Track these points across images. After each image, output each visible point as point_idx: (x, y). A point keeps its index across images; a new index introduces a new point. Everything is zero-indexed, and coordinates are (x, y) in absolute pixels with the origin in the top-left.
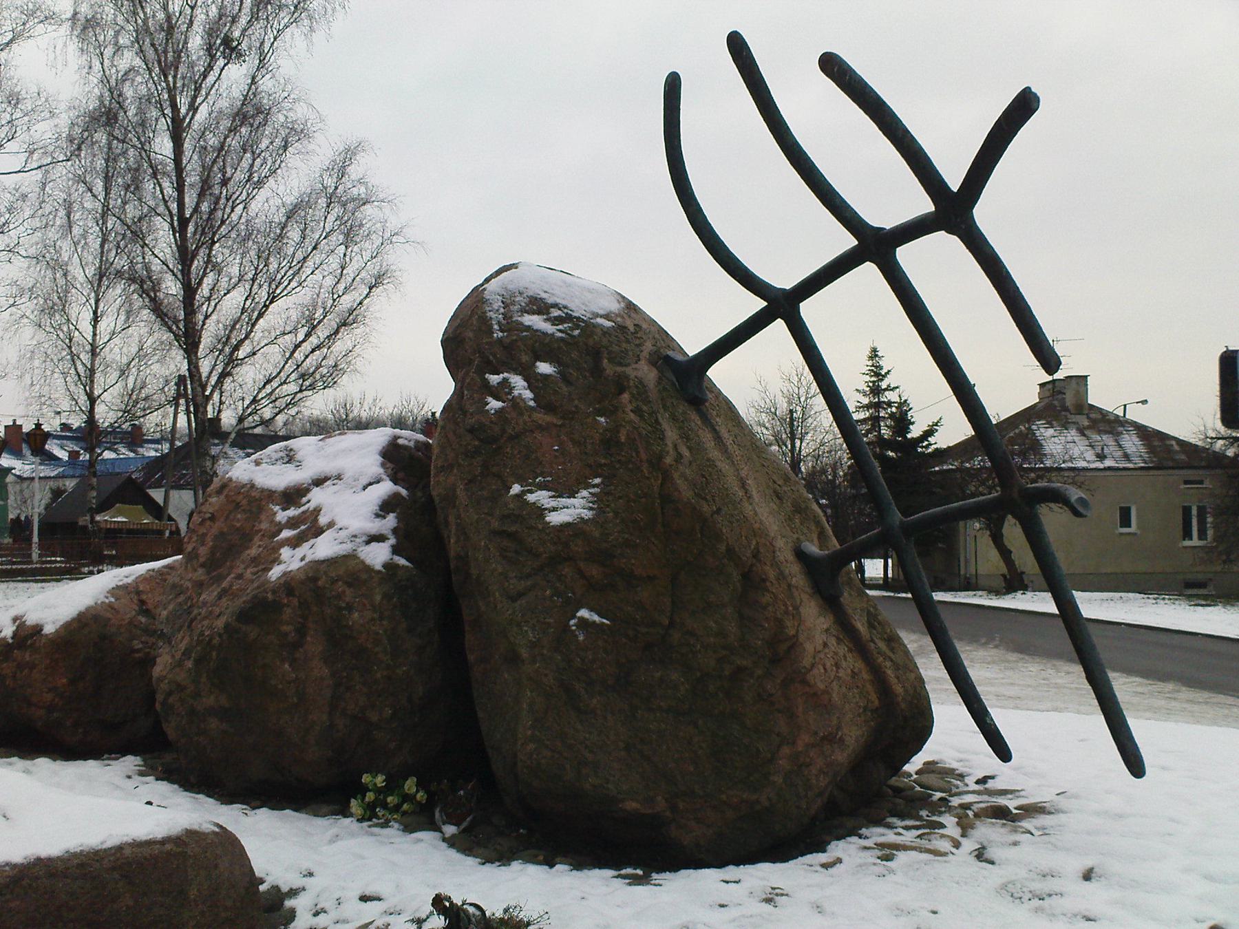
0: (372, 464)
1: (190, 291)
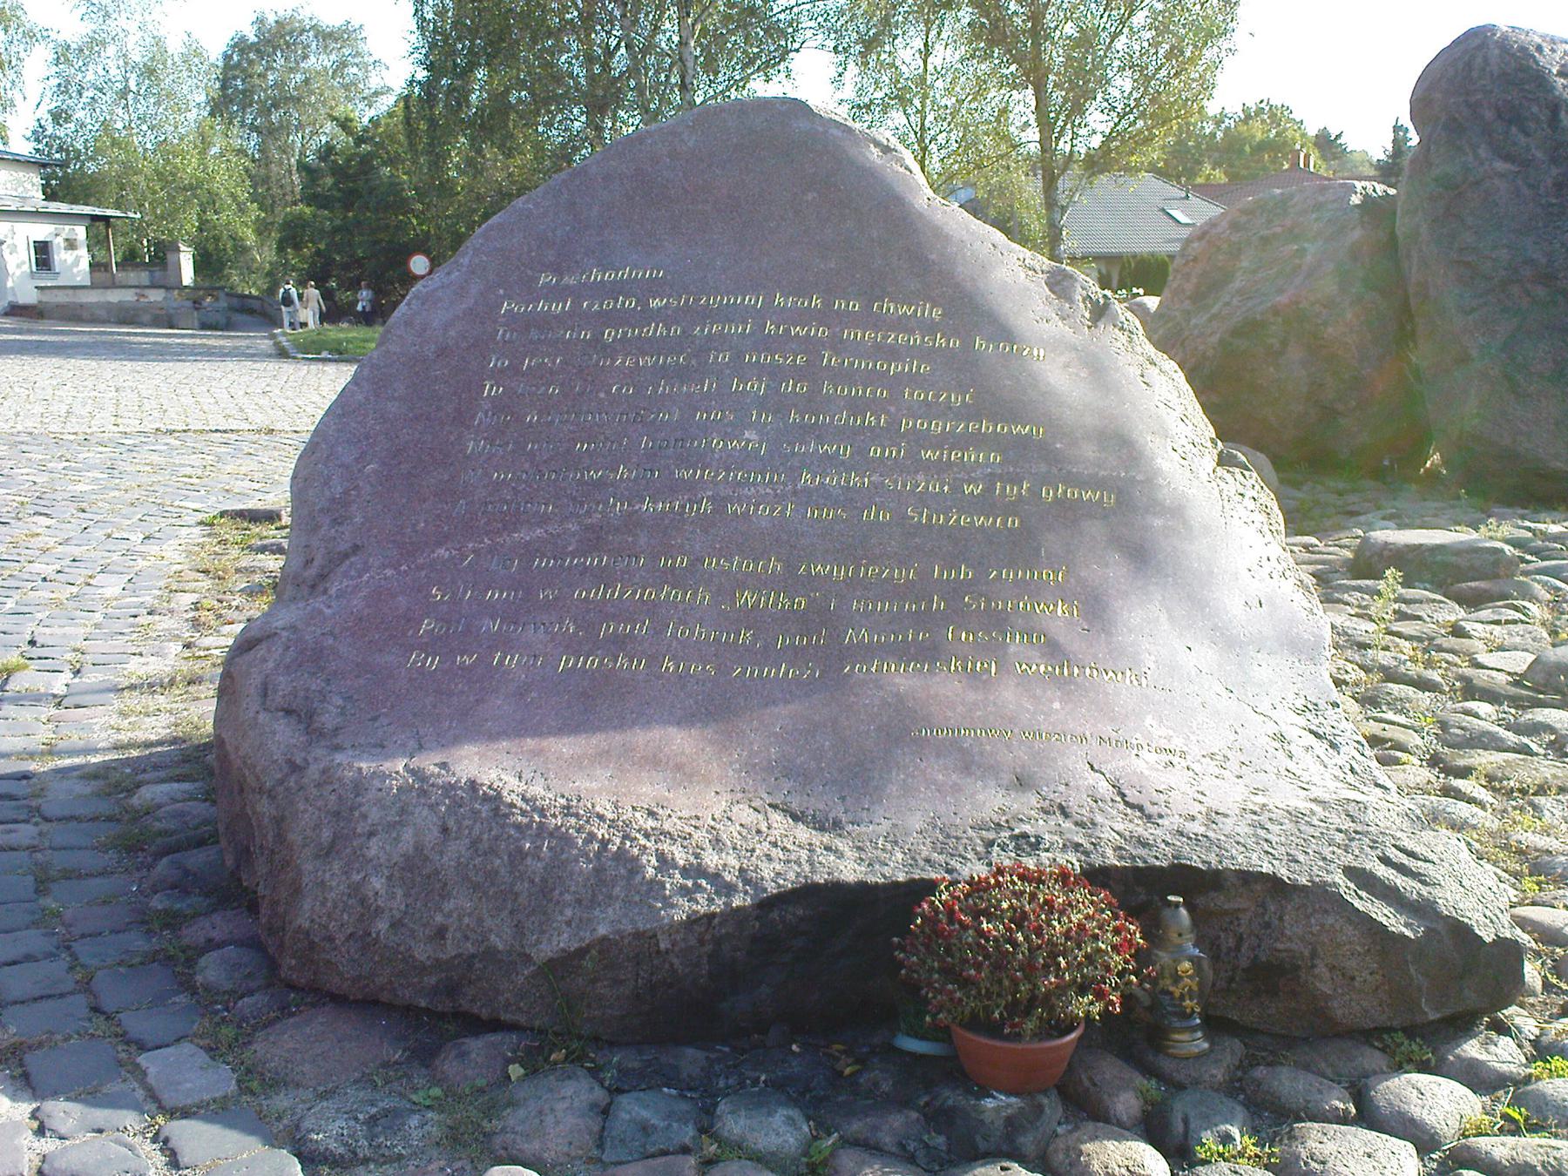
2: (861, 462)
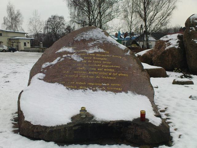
0: (176, 37)
1: (145, 13)
2: (97, 71)
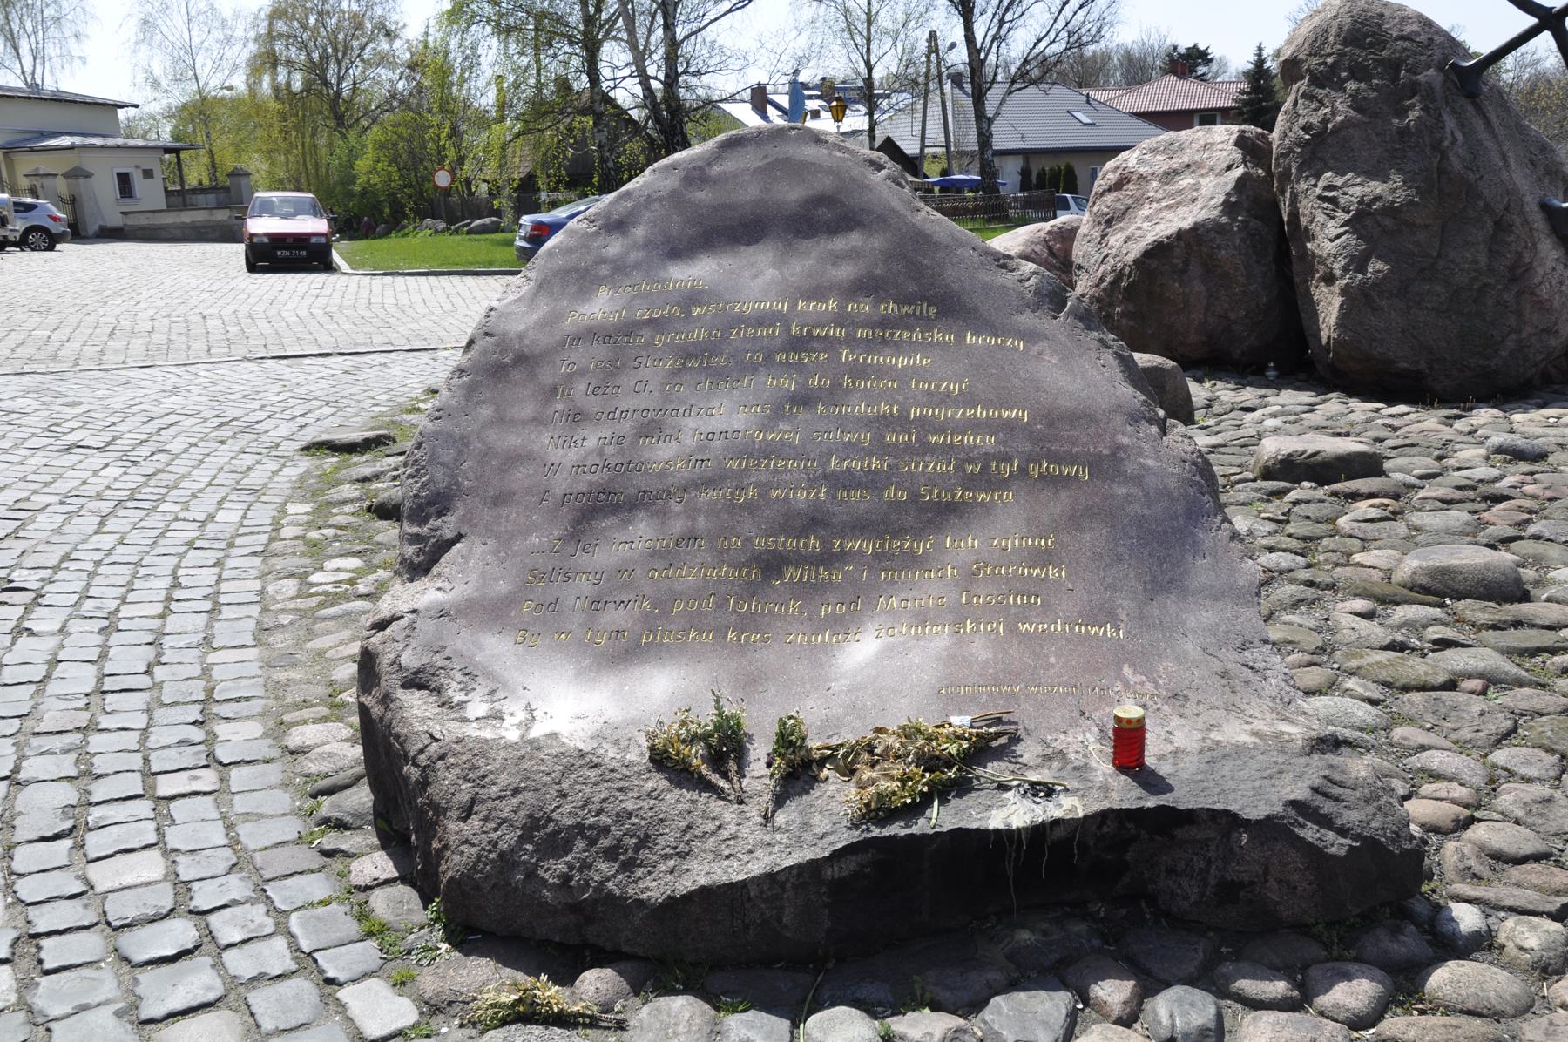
2: (881, 448)
